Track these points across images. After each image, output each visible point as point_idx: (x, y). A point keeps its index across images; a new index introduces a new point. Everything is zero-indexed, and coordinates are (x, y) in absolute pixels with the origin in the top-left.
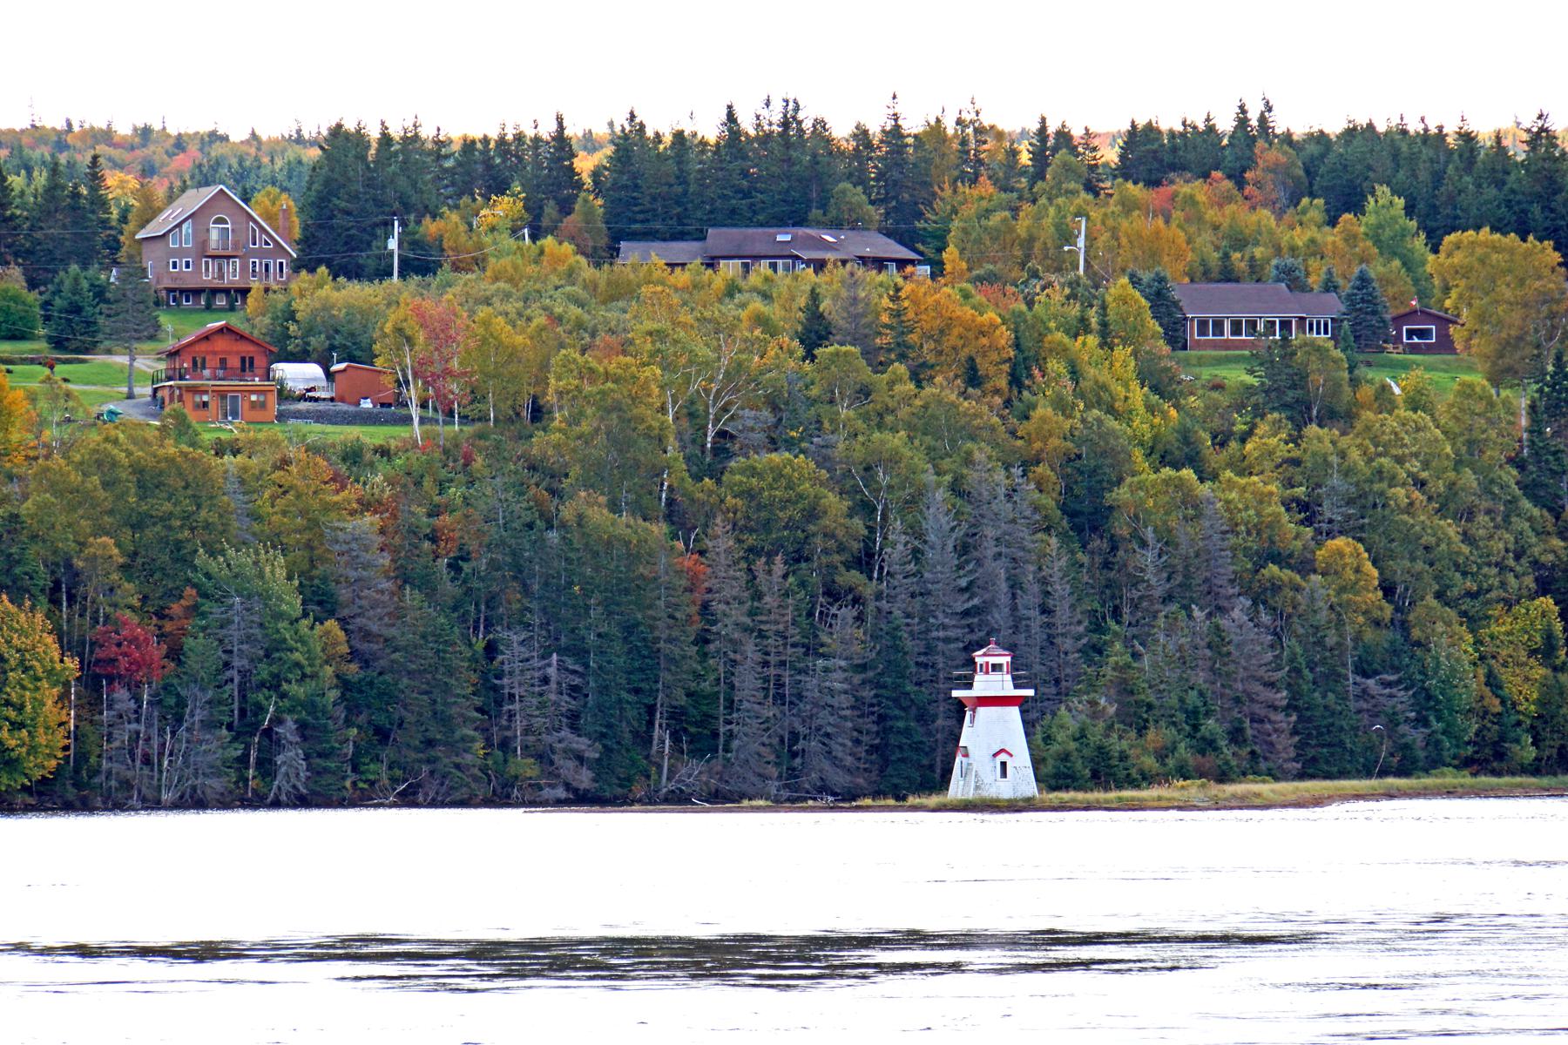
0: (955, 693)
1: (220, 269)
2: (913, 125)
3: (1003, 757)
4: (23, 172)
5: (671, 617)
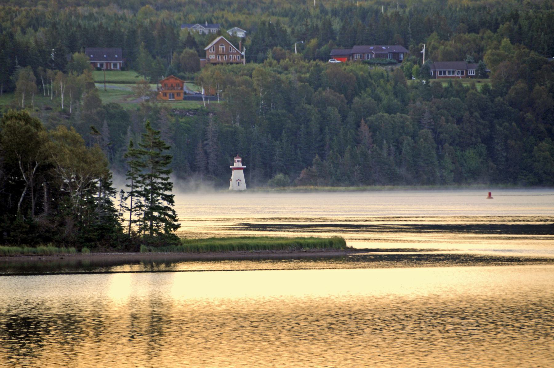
1: (222, 57)
3: (239, 181)
4: (512, 20)
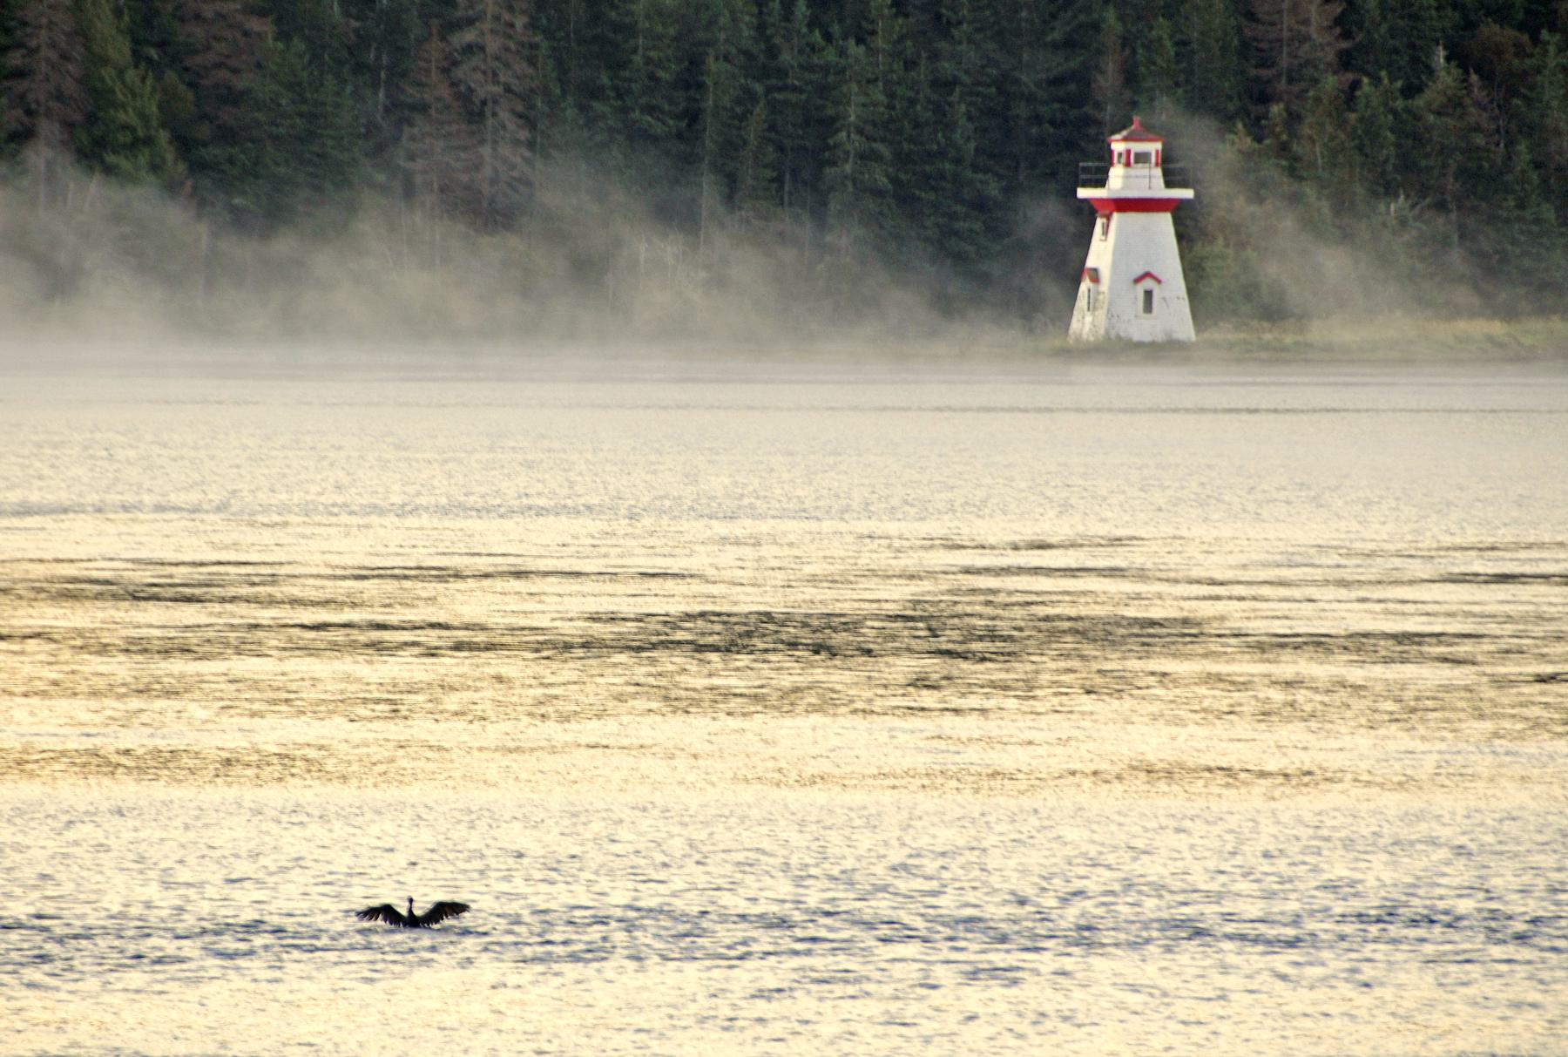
0: (1083, 193)
3: (1148, 284)
5: (652, 77)
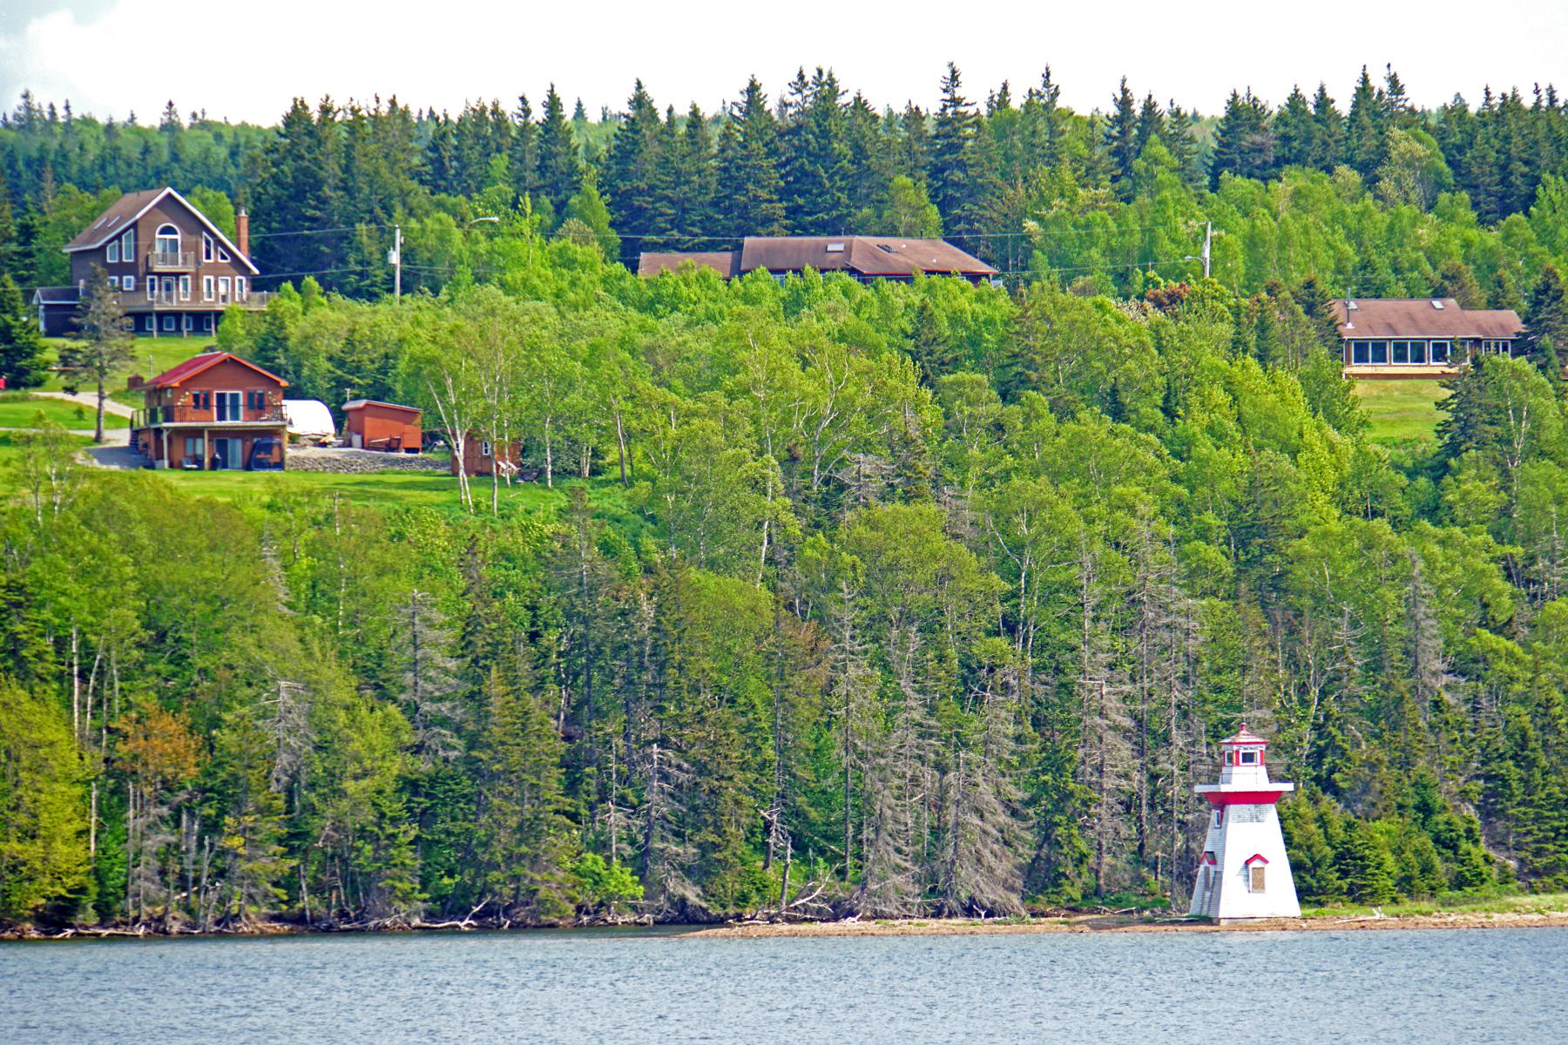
2: (976, 95)
